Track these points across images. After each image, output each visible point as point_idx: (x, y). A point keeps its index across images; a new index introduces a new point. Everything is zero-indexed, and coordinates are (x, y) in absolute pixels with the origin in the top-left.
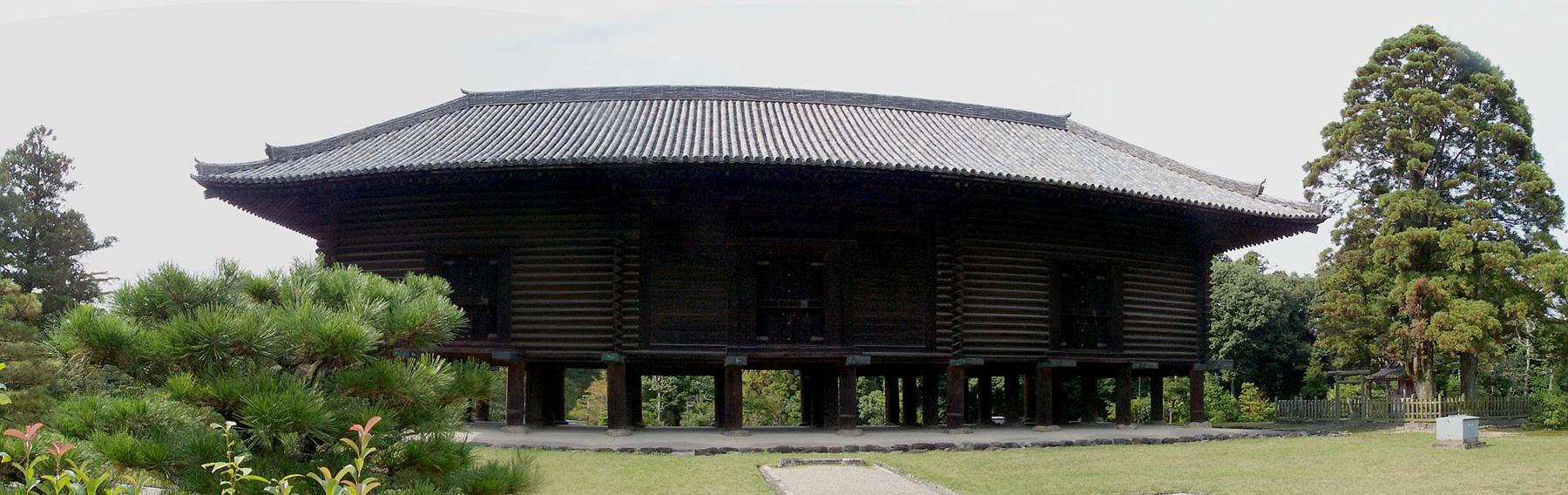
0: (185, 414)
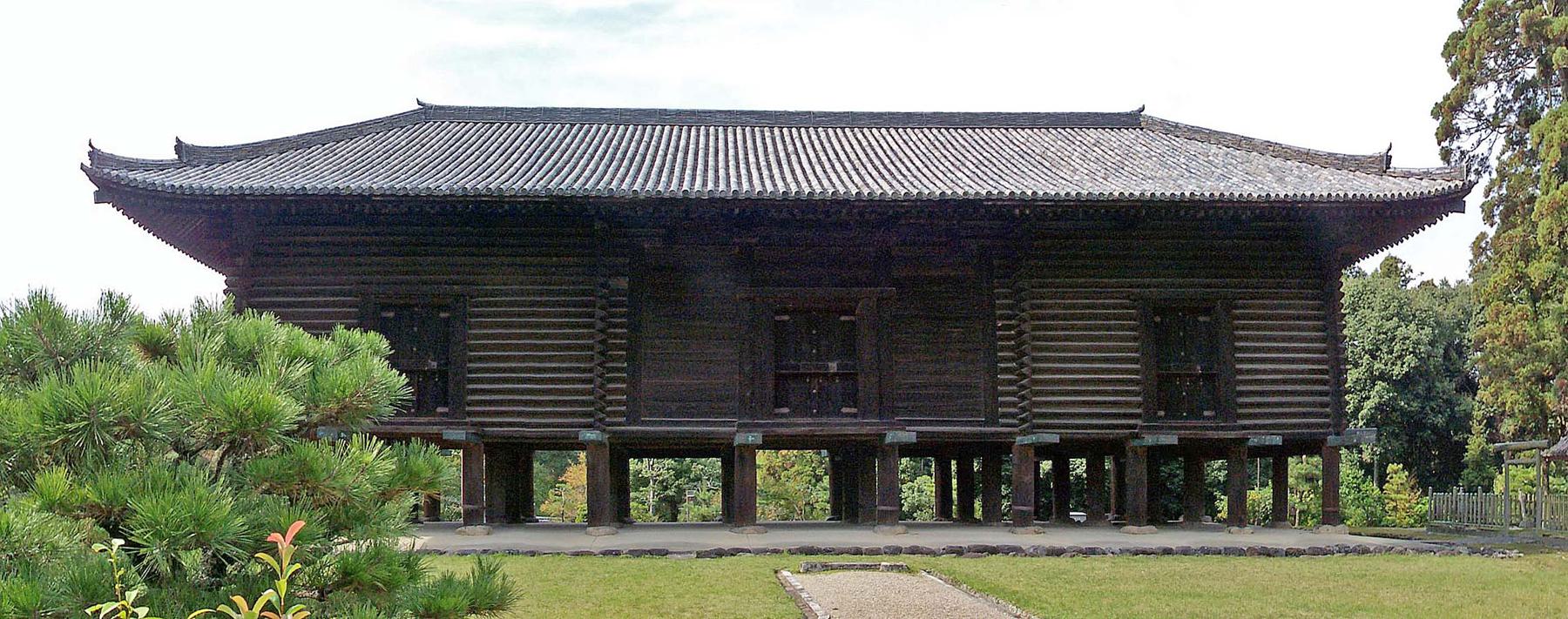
0: (61, 534)
